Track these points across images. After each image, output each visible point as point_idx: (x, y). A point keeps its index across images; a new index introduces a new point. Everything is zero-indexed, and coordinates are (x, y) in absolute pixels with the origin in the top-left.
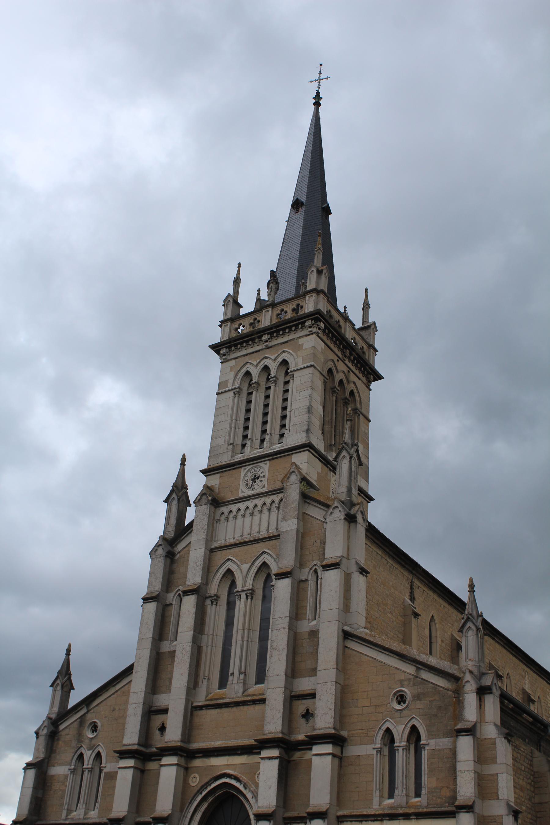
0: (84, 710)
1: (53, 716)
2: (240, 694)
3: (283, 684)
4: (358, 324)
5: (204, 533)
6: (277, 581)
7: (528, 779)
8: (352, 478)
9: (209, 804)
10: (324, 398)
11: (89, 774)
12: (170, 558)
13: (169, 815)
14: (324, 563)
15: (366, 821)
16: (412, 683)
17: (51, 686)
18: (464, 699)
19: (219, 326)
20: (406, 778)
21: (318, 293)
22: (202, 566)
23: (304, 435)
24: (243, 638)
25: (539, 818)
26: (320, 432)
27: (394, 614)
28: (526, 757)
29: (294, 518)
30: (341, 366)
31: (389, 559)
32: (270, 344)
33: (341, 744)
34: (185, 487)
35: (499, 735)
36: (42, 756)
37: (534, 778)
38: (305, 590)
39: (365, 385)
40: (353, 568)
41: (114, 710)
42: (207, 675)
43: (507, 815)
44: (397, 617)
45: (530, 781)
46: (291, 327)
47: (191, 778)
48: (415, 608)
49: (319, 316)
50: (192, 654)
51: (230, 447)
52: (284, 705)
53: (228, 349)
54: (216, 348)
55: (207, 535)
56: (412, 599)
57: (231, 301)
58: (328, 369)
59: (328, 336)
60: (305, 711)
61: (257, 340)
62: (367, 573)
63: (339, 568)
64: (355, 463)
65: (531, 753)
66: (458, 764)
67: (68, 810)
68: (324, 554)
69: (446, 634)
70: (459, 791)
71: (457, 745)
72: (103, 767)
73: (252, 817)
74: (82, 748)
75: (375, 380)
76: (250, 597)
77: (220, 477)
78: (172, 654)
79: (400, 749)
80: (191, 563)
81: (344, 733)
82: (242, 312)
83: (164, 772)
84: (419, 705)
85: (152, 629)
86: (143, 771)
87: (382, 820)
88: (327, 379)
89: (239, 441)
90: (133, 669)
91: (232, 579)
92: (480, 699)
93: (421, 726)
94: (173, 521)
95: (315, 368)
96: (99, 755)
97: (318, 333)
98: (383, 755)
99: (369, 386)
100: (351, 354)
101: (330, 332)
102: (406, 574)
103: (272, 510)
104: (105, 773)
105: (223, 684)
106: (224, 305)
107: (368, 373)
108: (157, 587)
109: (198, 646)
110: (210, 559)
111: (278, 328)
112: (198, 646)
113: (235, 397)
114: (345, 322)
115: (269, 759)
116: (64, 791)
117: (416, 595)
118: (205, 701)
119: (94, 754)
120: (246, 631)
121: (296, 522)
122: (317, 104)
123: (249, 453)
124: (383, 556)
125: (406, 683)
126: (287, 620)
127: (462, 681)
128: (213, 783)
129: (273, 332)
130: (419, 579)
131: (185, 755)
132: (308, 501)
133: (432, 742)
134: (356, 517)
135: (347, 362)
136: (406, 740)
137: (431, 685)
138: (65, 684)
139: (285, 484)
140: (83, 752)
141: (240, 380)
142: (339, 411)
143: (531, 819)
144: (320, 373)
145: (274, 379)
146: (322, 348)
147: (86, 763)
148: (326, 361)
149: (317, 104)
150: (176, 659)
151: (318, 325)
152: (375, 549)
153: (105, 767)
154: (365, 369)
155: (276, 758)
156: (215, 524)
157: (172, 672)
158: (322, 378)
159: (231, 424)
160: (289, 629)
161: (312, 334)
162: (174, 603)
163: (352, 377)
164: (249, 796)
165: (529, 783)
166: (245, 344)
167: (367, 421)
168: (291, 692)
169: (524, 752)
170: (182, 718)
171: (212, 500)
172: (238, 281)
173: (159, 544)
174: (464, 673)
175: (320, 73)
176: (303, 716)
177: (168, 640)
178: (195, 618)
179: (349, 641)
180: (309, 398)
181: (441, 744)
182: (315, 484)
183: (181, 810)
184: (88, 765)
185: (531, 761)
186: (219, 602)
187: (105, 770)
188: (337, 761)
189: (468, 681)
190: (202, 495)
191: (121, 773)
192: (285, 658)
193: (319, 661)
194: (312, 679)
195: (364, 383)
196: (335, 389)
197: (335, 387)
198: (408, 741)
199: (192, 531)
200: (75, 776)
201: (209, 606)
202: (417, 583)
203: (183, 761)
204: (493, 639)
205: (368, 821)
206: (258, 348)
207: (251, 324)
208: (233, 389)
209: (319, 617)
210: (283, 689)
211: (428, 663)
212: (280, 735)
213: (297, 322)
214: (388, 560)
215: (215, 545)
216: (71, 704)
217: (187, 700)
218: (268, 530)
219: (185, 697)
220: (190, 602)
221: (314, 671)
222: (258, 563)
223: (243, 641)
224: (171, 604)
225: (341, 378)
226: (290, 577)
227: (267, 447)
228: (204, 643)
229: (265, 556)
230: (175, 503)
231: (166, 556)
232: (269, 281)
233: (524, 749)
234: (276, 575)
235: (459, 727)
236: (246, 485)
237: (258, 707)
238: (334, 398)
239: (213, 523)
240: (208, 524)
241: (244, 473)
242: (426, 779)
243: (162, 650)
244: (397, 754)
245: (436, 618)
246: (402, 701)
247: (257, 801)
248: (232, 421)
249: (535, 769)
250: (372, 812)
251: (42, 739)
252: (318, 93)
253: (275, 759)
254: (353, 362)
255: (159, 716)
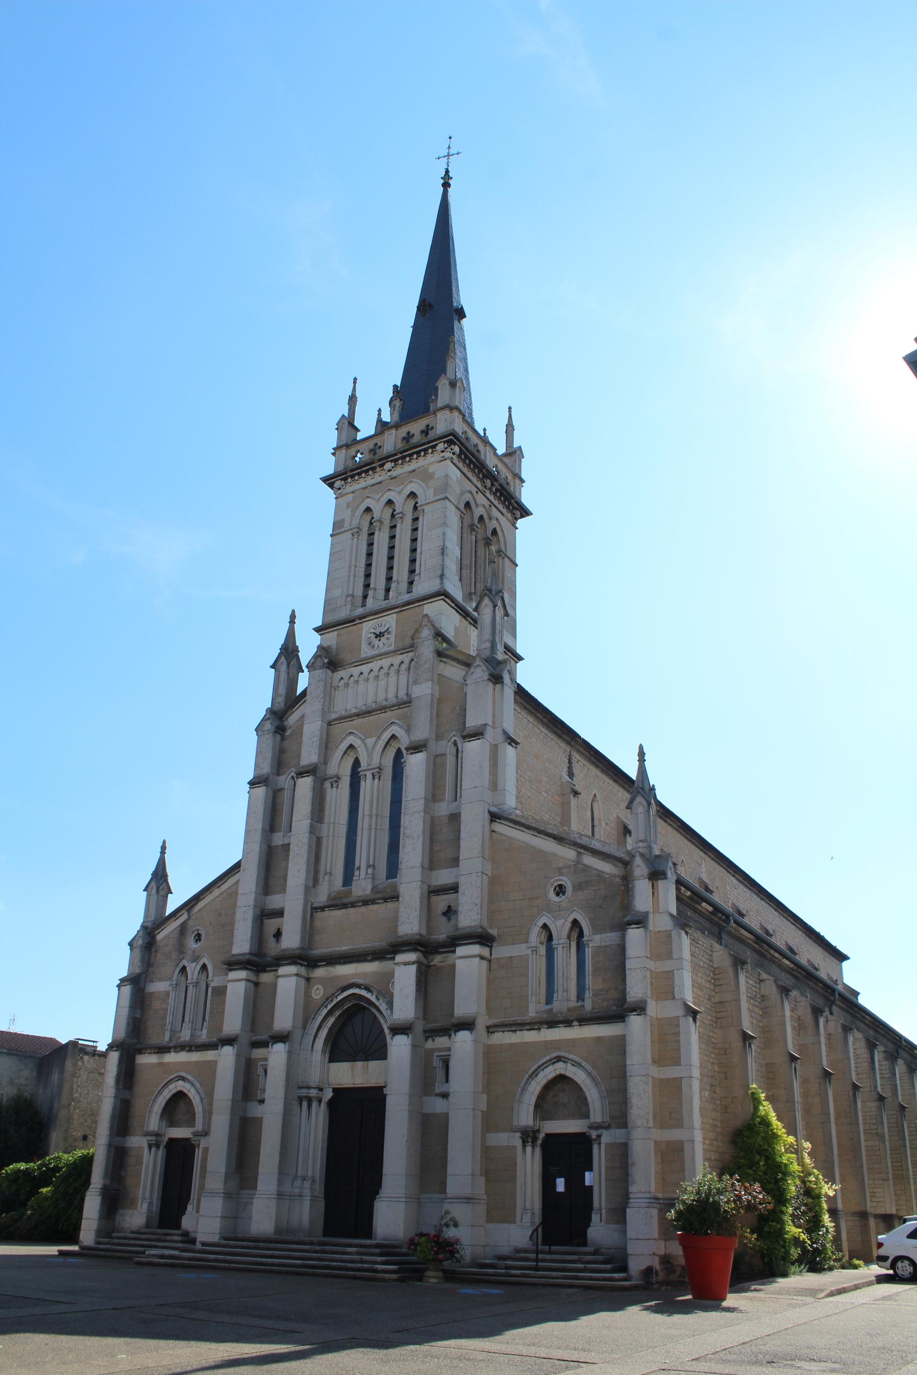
0: (185, 916)
1: (149, 925)
2: (368, 892)
3: (419, 877)
4: (501, 450)
5: (320, 702)
6: (410, 756)
7: (707, 976)
8: (497, 631)
9: (337, 1019)
10: (462, 528)
11: (194, 990)
12: (280, 734)
13: (289, 1033)
14: (464, 734)
15: (520, 1030)
16: (572, 870)
17: (144, 890)
18: (633, 887)
19: (332, 454)
20: (566, 980)
21: (451, 410)
22: (318, 742)
23: (438, 581)
24: (370, 825)
25: (720, 1018)
26: (457, 578)
27: (550, 792)
28: (705, 951)
29: (427, 680)
30: (480, 499)
31: (543, 727)
32: (394, 473)
33: (490, 944)
34: (296, 650)
35: (675, 926)
36: (138, 971)
37: (714, 974)
38: (443, 765)
39: (510, 522)
40: (501, 738)
41: (220, 915)
42: (328, 870)
43: (684, 1016)
44: (554, 797)
45: (709, 978)
46: (411, 455)
47: (313, 990)
48: (574, 785)
49: (453, 438)
50: (310, 846)
51: (349, 599)
52: (421, 902)
53: (343, 482)
54: (329, 481)
55: (323, 705)
56: (571, 774)
57: (347, 423)
58: (465, 502)
59: (464, 462)
60: (446, 908)
61: (378, 469)
62: (517, 743)
63: (483, 738)
64: (499, 612)
65: (711, 947)
66: (627, 961)
67: (171, 1031)
68: (464, 723)
69: (610, 816)
70: (629, 992)
71: (627, 940)
72: (209, 981)
73: (387, 1031)
74: (184, 960)
75: (522, 516)
76: (377, 777)
77: (338, 635)
78: (286, 847)
79: (560, 948)
80: (306, 738)
81: (493, 932)
82: (360, 436)
83: (281, 981)
84: (581, 895)
85: (261, 819)
86: (256, 984)
87: (539, 1029)
88: (465, 515)
89: (359, 592)
90: (240, 867)
91: (355, 757)
92: (653, 886)
93: (584, 920)
94: (282, 690)
95: (449, 500)
96: (204, 967)
97: (452, 458)
98: (540, 955)
99: (515, 523)
100: (493, 485)
101: (467, 457)
102: (563, 745)
103: (401, 673)
104: (213, 988)
105: (348, 879)
106: (337, 429)
107: (514, 508)
108: (266, 769)
109: (317, 837)
110: (328, 734)
111: (403, 454)
112: (317, 837)
113: (353, 539)
114: (485, 446)
115: (406, 965)
116: (166, 1010)
117: (576, 770)
118: (328, 901)
119: (199, 967)
120: (374, 817)
121: (431, 686)
122: (446, 185)
123: (371, 604)
124: (536, 724)
125: (565, 871)
126: (422, 802)
127: (631, 866)
128: (340, 994)
129: (397, 460)
130: (578, 751)
131: (306, 963)
132: (444, 660)
133: (597, 938)
134: (502, 678)
135: (488, 494)
136: (566, 937)
137: (595, 872)
138: (161, 887)
139: (416, 641)
140: (186, 964)
141: (359, 518)
142: (479, 553)
143: (711, 1020)
144: (456, 507)
145: (401, 515)
146: (457, 477)
147: (189, 977)
148: (462, 493)
149: (446, 185)
150: (291, 853)
151: (452, 449)
152: (525, 716)
153: (212, 981)
154: (510, 504)
155: (413, 963)
156: (333, 693)
157: (286, 869)
158: (460, 513)
159: (350, 572)
160: (425, 812)
161: (446, 459)
162: (286, 787)
163: (495, 513)
164: (383, 1007)
165: (708, 981)
166: (363, 475)
167: (513, 566)
168: (430, 887)
169: (703, 946)
170: (300, 921)
171: (328, 663)
172: (353, 399)
173: (266, 717)
174: (633, 856)
175: (449, 148)
176: (444, 914)
177: (280, 831)
178: (313, 804)
179: (497, 824)
180: (443, 537)
181: (607, 940)
182: (452, 639)
183: (304, 1027)
184: (192, 979)
185: (711, 956)
186: (340, 784)
187: (212, 984)
188: (485, 964)
189: (638, 866)
190: (315, 657)
191: (231, 987)
192: (421, 847)
193: (461, 849)
194: (454, 870)
195: (508, 520)
196: (475, 527)
197: (474, 525)
198: (569, 937)
199: (305, 701)
200: (177, 992)
201: (329, 790)
202: (576, 756)
203: (252, 977)
204: (666, 821)
205: (522, 1030)
206: (379, 479)
207: (371, 451)
208: (351, 529)
209: (461, 797)
210: (419, 883)
211: (591, 846)
212: (418, 937)
213: (427, 446)
214: (541, 728)
215: (334, 716)
216: (169, 910)
217: (306, 900)
218: (397, 697)
219: (303, 896)
220: (305, 784)
221: (455, 862)
222: (386, 736)
223: (370, 829)
224: (283, 789)
225: (481, 514)
226: (425, 750)
227: (393, 597)
228: (324, 834)
229: (394, 727)
230: (283, 668)
231: (276, 732)
232: (392, 398)
233: (703, 943)
234: (407, 749)
235: (628, 919)
236: (372, 647)
237: (390, 905)
238: (474, 537)
239: (331, 691)
240: (324, 692)
241: (368, 627)
242: (590, 980)
243: (274, 844)
244: (556, 953)
245: (598, 797)
246: (561, 892)
247: (392, 1012)
248: (350, 567)
249: (715, 966)
250: (527, 1019)
251: (137, 951)
252: (447, 171)
253: (412, 964)
254: (495, 494)
255: (274, 920)
